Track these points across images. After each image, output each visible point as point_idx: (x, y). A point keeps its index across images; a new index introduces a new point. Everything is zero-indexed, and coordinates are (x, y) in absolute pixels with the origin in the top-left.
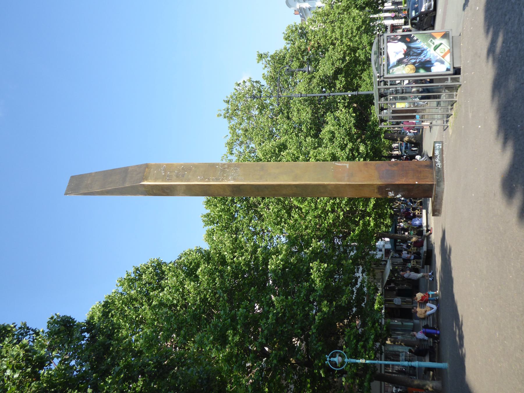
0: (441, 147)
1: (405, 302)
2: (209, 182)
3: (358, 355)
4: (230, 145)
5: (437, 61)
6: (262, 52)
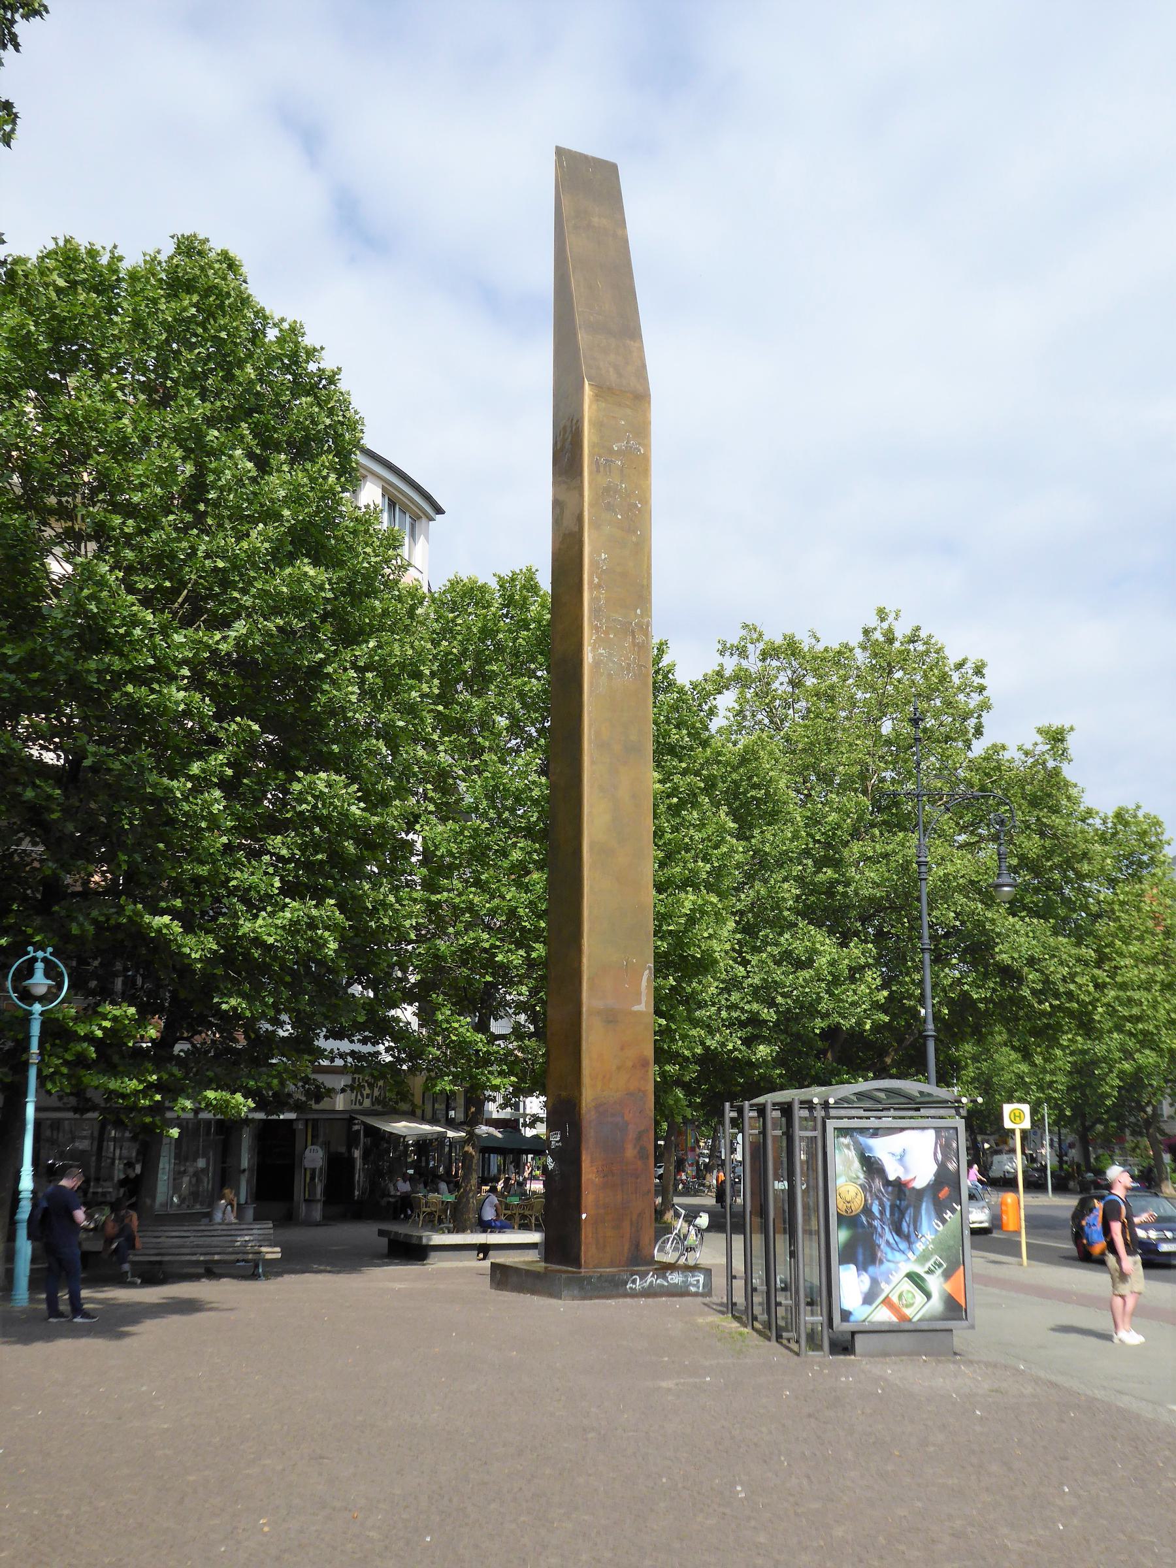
0: (693, 1289)
1: (313, 1178)
2: (590, 589)
3: (57, 1041)
4: (792, 648)
5: (875, 1282)
6: (1071, 741)
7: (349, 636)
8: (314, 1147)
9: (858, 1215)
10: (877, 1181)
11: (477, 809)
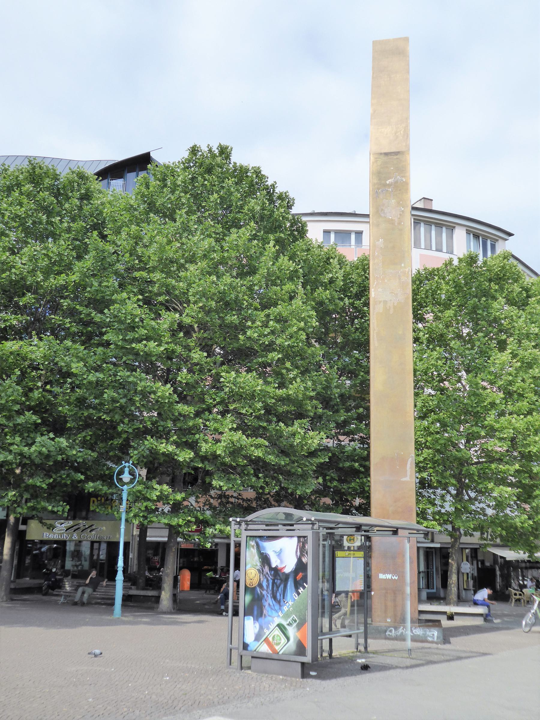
0: (430, 639)
5: (261, 628)
9: (255, 587)
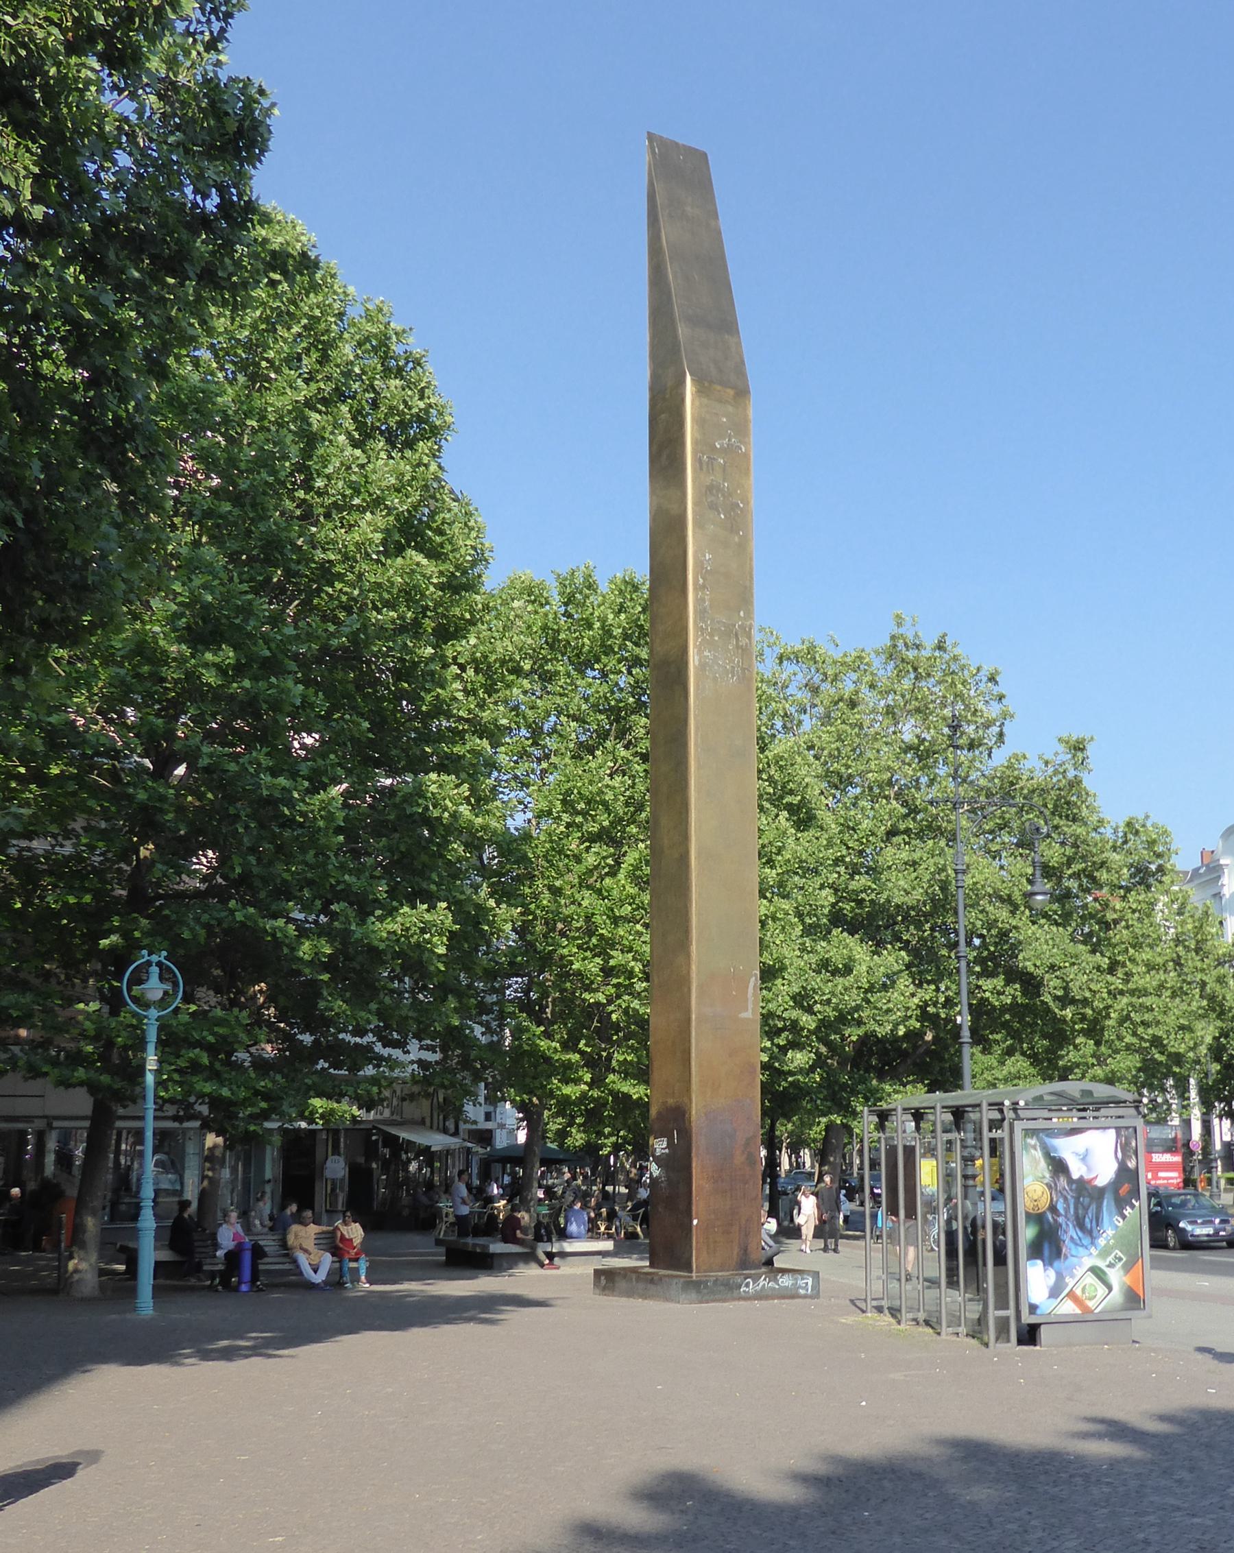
0: (802, 1292)
2: (695, 589)
5: (1060, 1277)
6: (1091, 750)
7: (447, 632)
8: (336, 1157)
9: (1044, 1213)
10: (1062, 1179)
11: (550, 813)
